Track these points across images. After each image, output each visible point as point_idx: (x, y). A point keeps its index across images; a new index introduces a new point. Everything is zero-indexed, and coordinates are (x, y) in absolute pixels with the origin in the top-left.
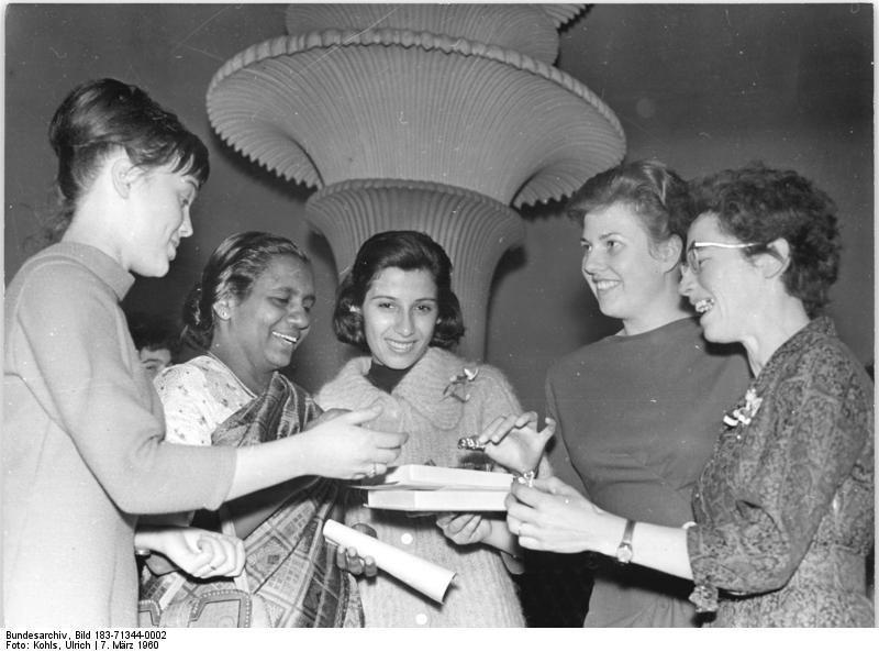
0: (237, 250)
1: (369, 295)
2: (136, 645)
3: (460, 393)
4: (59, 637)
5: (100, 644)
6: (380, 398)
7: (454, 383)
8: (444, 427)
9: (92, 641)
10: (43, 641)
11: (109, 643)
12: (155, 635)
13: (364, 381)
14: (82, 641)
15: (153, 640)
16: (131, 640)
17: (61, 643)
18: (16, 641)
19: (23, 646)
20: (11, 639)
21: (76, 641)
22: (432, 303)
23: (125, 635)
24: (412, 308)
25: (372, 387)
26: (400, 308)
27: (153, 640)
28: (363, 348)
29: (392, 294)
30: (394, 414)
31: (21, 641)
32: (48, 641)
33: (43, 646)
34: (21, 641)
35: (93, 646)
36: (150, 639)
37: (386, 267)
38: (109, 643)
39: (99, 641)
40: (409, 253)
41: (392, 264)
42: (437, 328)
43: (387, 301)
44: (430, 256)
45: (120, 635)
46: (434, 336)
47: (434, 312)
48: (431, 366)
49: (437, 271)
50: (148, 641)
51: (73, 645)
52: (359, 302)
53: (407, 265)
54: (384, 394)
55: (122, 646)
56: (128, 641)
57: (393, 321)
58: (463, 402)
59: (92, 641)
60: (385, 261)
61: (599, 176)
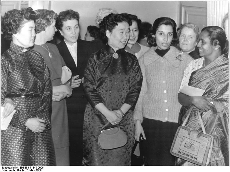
0: (182, 114)
1: (157, 32)
2: (36, 170)
3: (179, 58)
4: (15, 168)
5: (26, 170)
6: (160, 58)
7: (178, 56)
8: (176, 67)
9: (24, 169)
10: (11, 169)
11: (29, 170)
12: (41, 168)
13: (155, 52)
14: (22, 169)
15: (40, 169)
16: (34, 169)
17: (16, 170)
18: (4, 169)
19: (6, 171)
20: (3, 169)
21: (20, 169)
22: (172, 33)
23: (33, 168)
24: (167, 35)
25: (158, 55)
26: (165, 35)
27: (40, 169)
28: (155, 45)
29: (163, 31)
30: (163, 62)
31: (5, 169)
32: (13, 169)
33: (11, 171)
34: (5, 169)
35: (24, 171)
36: (39, 169)
37: (161, 24)
38: (29, 170)
39: (26, 169)
40: (167, 21)
41: (163, 24)
42: (172, 41)
43: (161, 32)
44: (171, 22)
45: (31, 168)
46: (172, 43)
47: (172, 36)
48: (173, 51)
49: (173, 26)
50: (39, 169)
51: (19, 170)
52: (154, 34)
53: (166, 24)
54: (160, 57)
55: (32, 170)
56: (33, 169)
57: (163, 38)
58: (181, 61)
59: (24, 169)
60: (161, 23)
61: (190, 77)
